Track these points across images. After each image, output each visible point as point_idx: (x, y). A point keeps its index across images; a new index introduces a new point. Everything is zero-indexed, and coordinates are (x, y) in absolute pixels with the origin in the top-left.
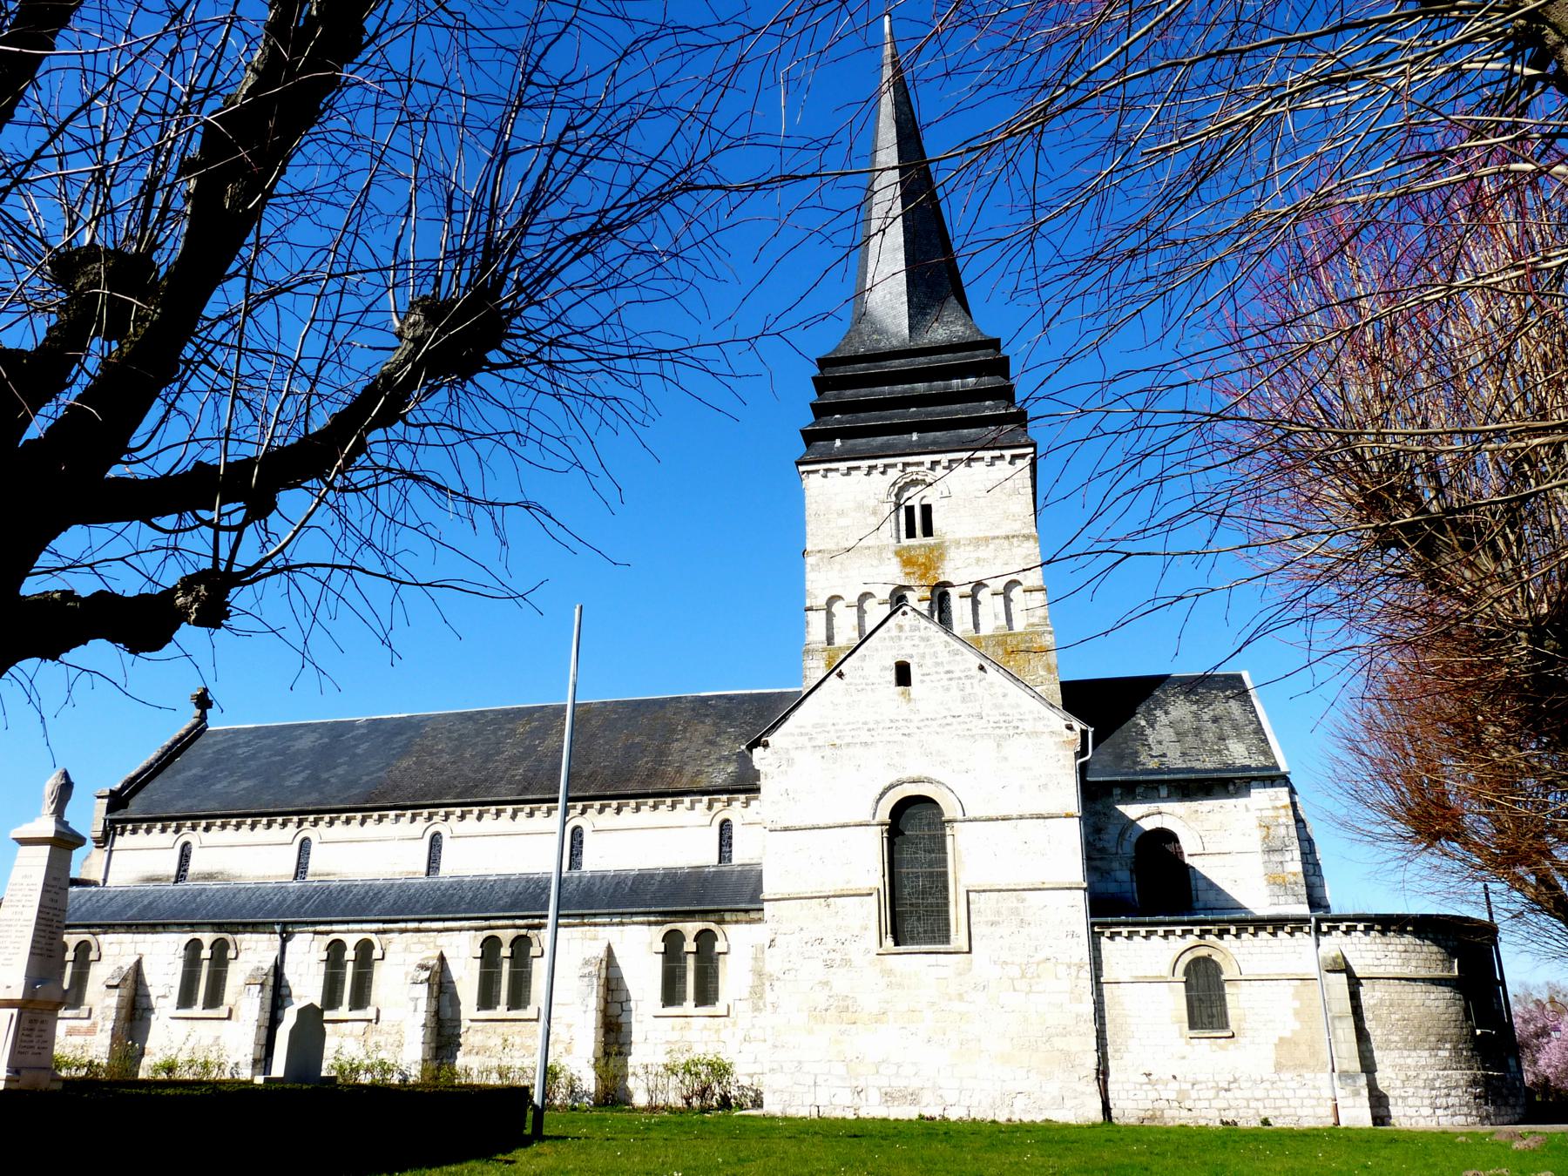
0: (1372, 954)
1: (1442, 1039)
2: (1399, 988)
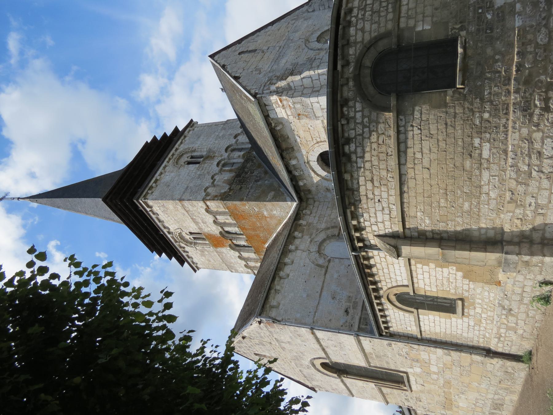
0: (379, 214)
1: (469, 152)
2: (412, 193)
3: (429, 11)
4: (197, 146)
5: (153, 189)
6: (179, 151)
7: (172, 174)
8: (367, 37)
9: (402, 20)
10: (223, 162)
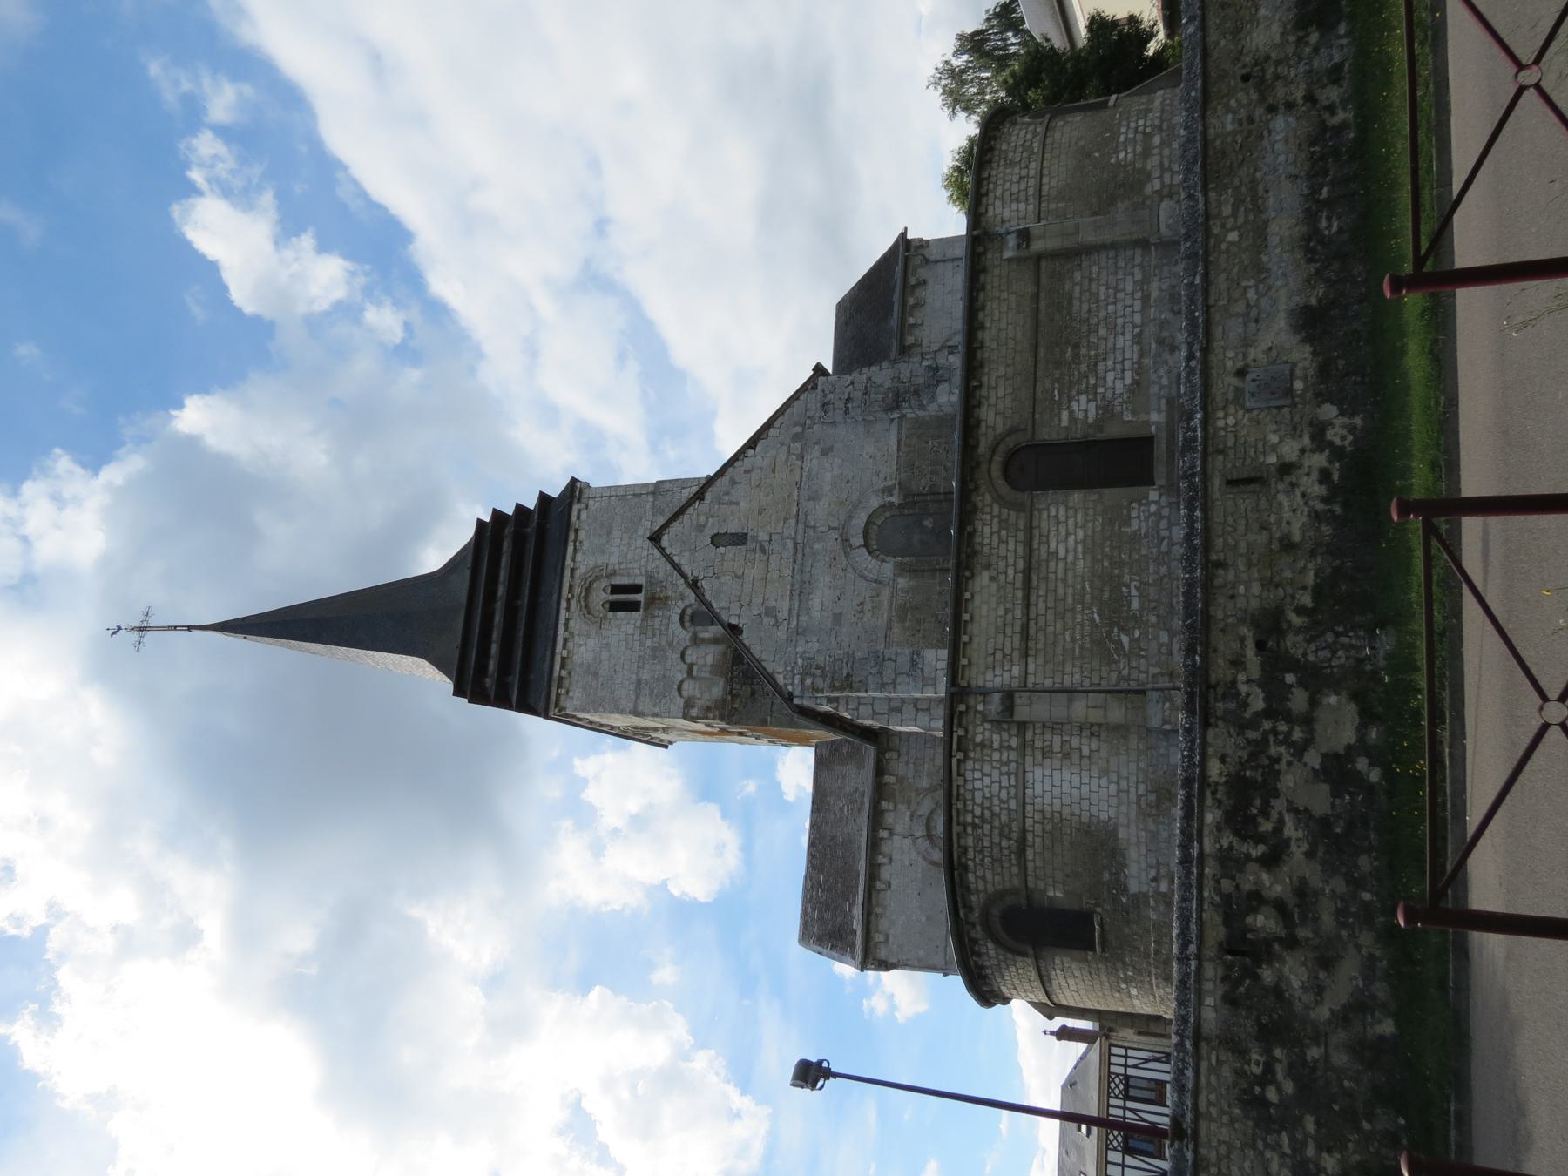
3: (1059, 876)
4: (614, 560)
5: (566, 683)
6: (577, 574)
7: (592, 643)
8: (990, 889)
9: (1021, 524)
10: (689, 611)
